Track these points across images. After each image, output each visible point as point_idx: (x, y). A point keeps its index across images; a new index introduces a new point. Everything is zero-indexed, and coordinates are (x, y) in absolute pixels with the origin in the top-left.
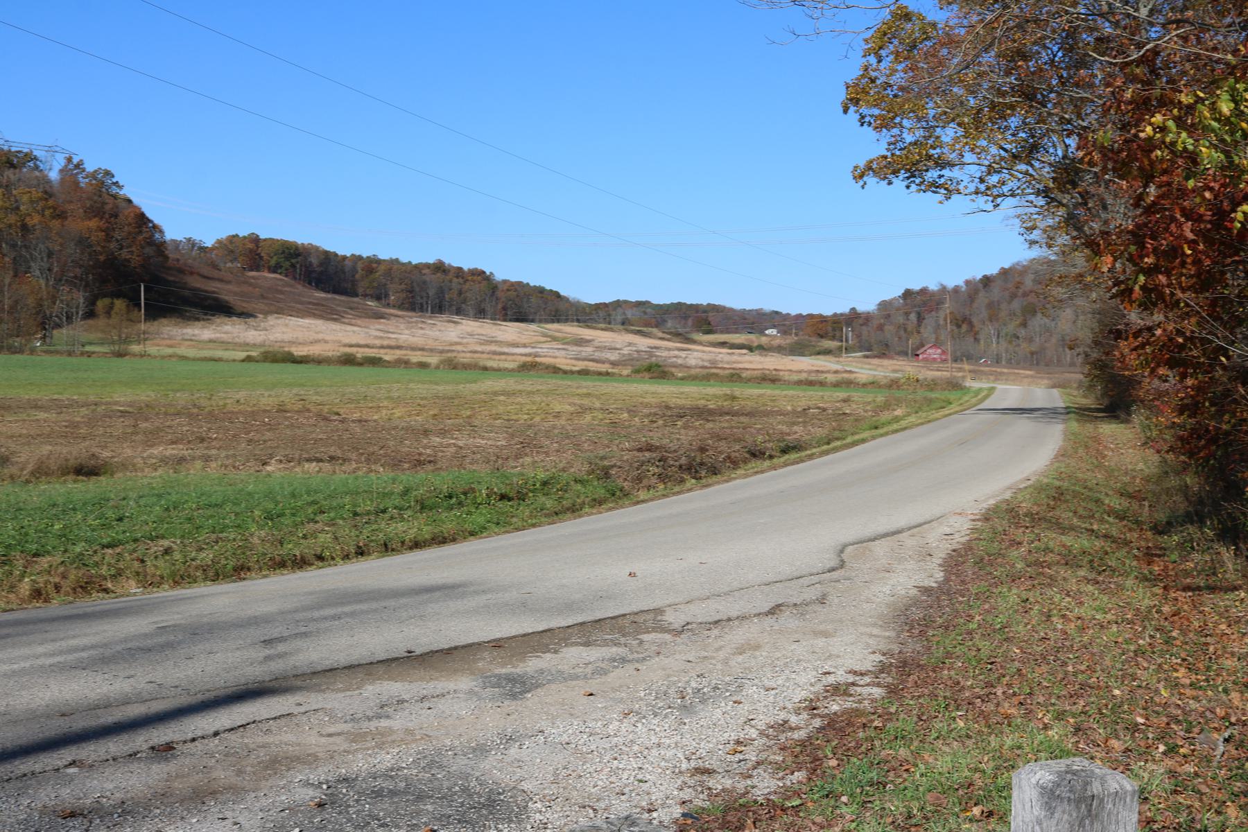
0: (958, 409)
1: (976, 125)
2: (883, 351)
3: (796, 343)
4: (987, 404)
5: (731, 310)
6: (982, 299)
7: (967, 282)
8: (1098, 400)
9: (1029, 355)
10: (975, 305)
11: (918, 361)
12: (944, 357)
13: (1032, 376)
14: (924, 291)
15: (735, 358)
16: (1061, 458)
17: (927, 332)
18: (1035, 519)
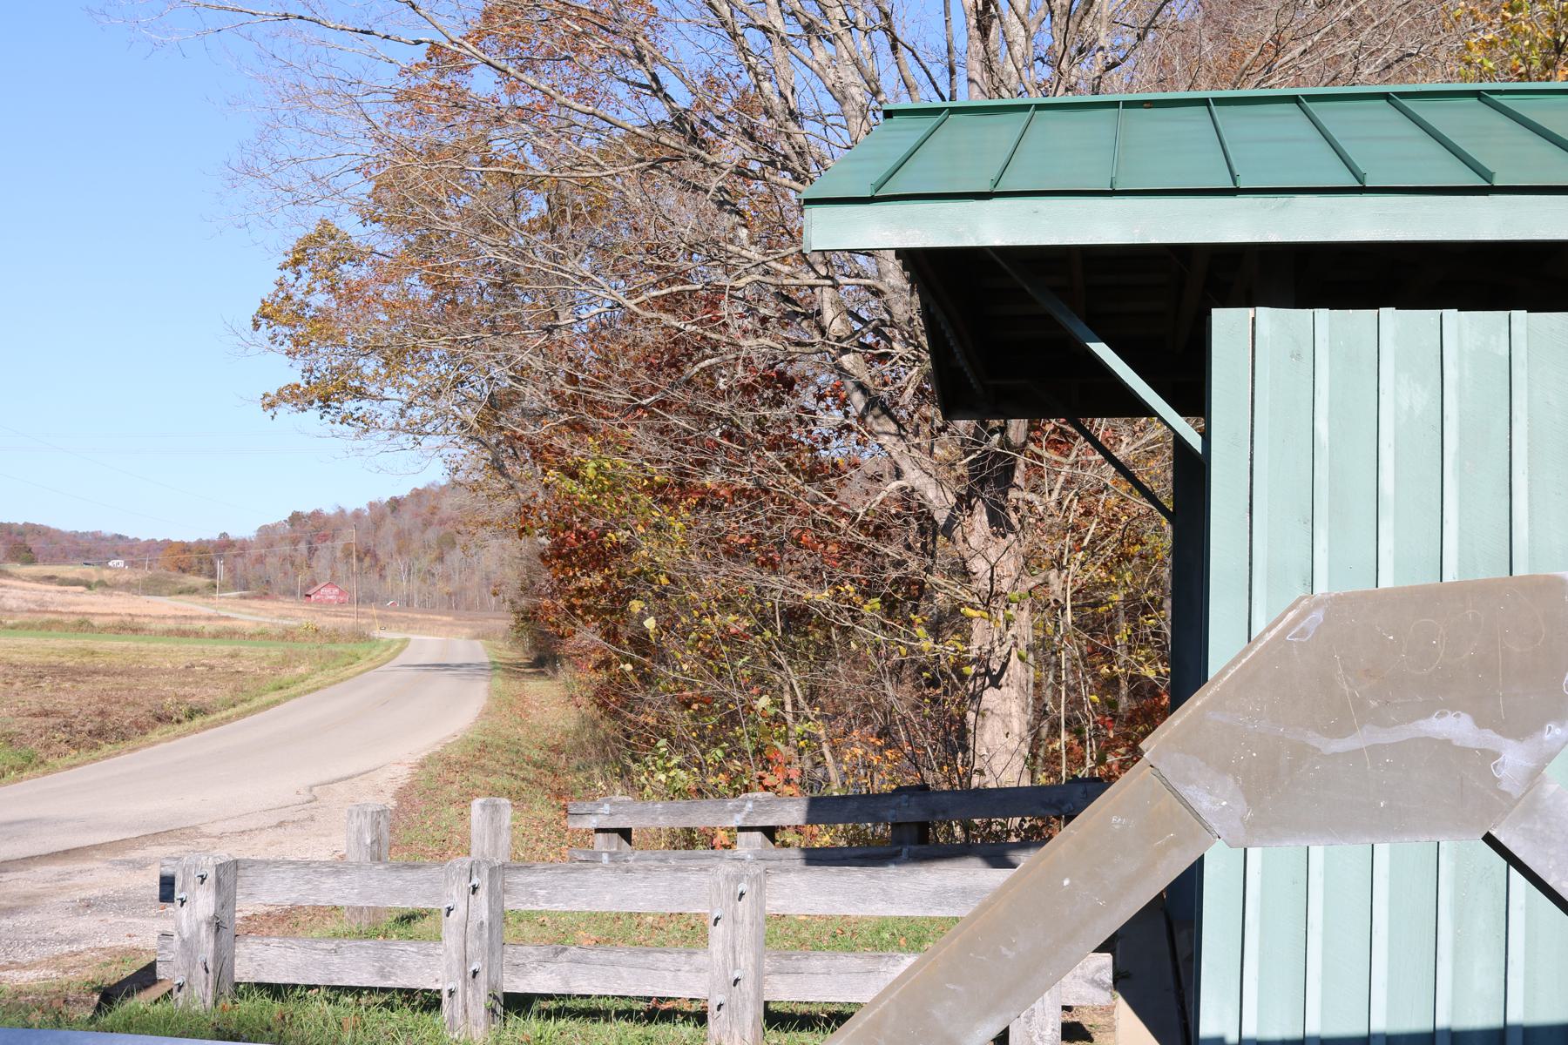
0: (370, 665)
1: (397, 357)
2: (264, 590)
3: (151, 579)
4: (401, 659)
5: (58, 532)
6: (389, 526)
7: (372, 505)
9: (447, 597)
10: (381, 533)
11: (309, 603)
12: (342, 598)
13: (451, 624)
14: (316, 515)
15: (69, 598)
16: (485, 716)
17: (321, 564)
18: (465, 767)
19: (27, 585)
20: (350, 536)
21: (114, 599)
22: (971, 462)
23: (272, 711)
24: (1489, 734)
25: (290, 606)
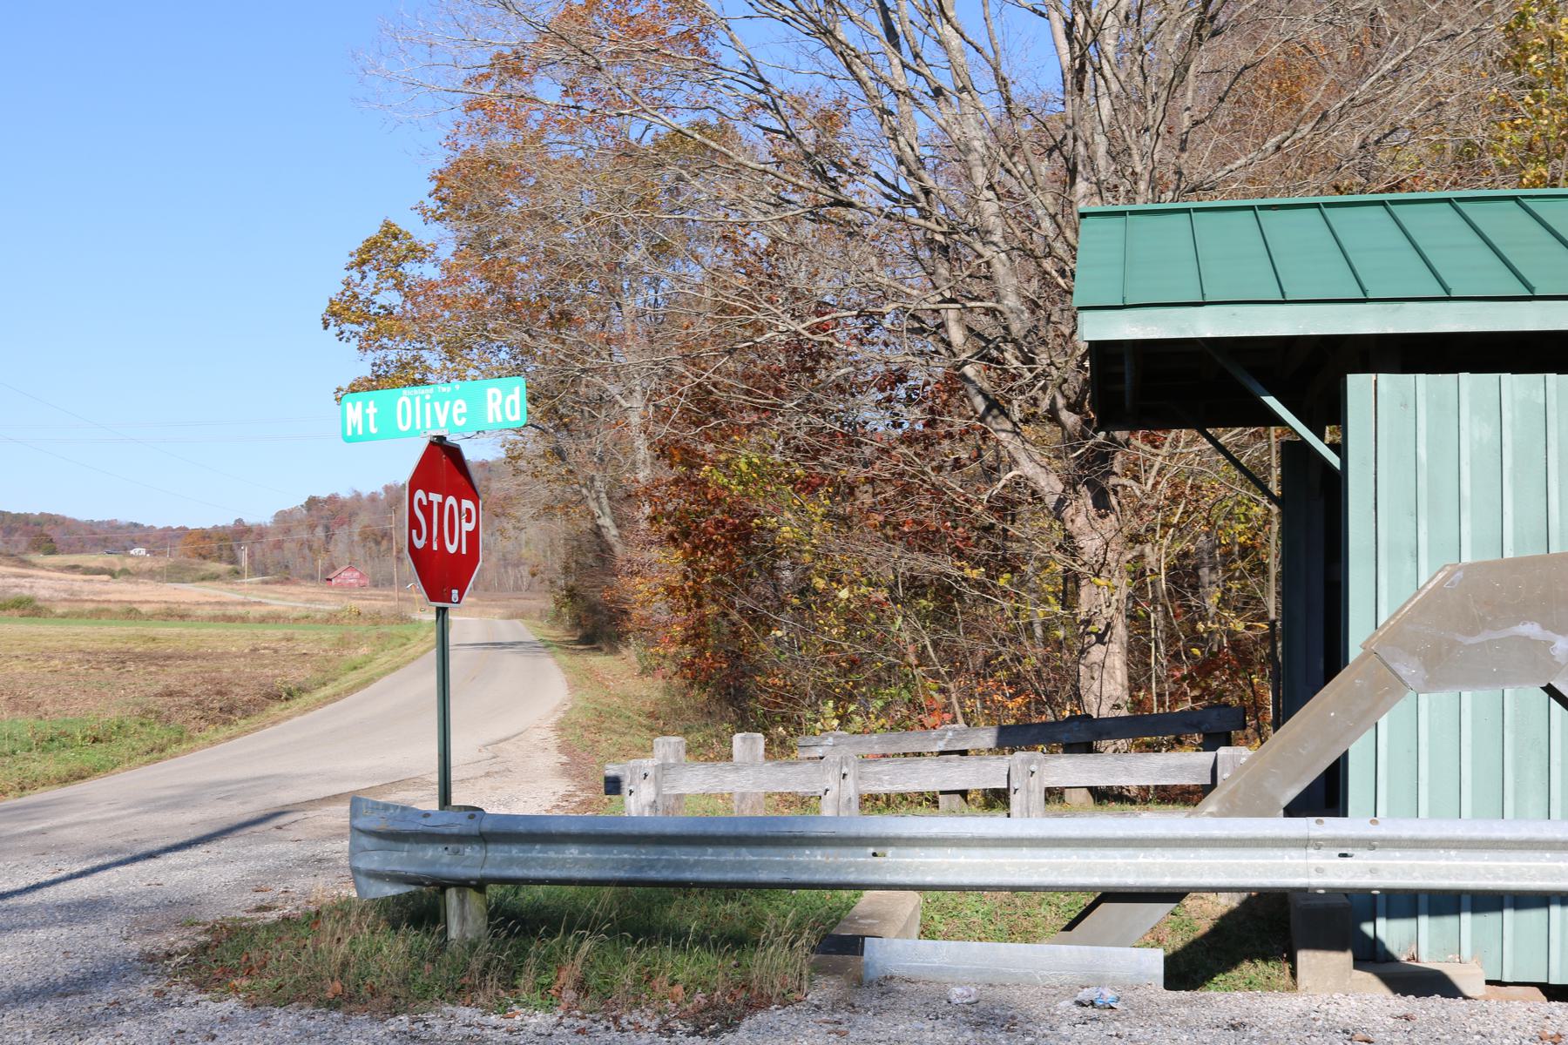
2: (284, 574)
7: (387, 489)
8: (568, 631)
12: (362, 582)
14: (332, 499)
15: (98, 587)
17: (339, 548)
19: (51, 574)
20: (364, 519)
21: (142, 587)
22: (1078, 457)
23: (374, 687)
24: (1549, 633)
25: (315, 590)
